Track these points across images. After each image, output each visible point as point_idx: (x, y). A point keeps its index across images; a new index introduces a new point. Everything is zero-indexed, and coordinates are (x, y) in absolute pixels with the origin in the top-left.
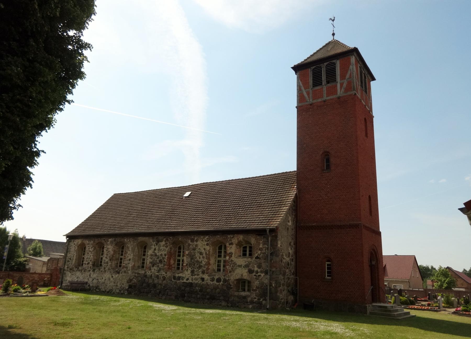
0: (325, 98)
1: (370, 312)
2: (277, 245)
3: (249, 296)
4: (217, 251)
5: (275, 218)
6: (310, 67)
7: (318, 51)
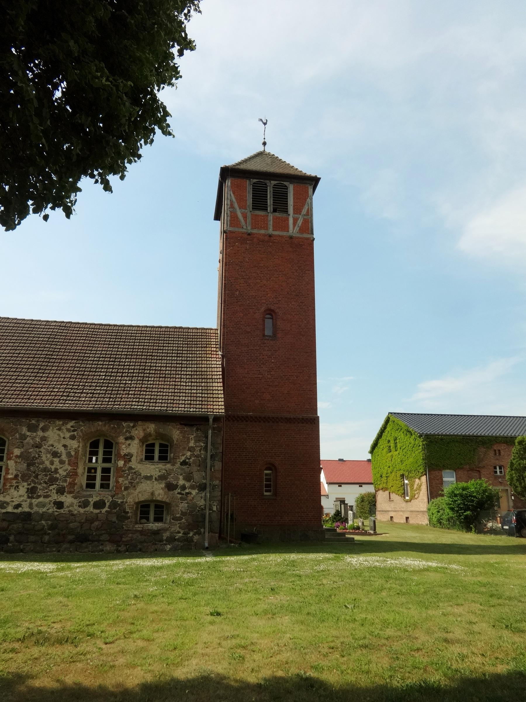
0: (271, 231)
3: (165, 530)
4: (88, 449)
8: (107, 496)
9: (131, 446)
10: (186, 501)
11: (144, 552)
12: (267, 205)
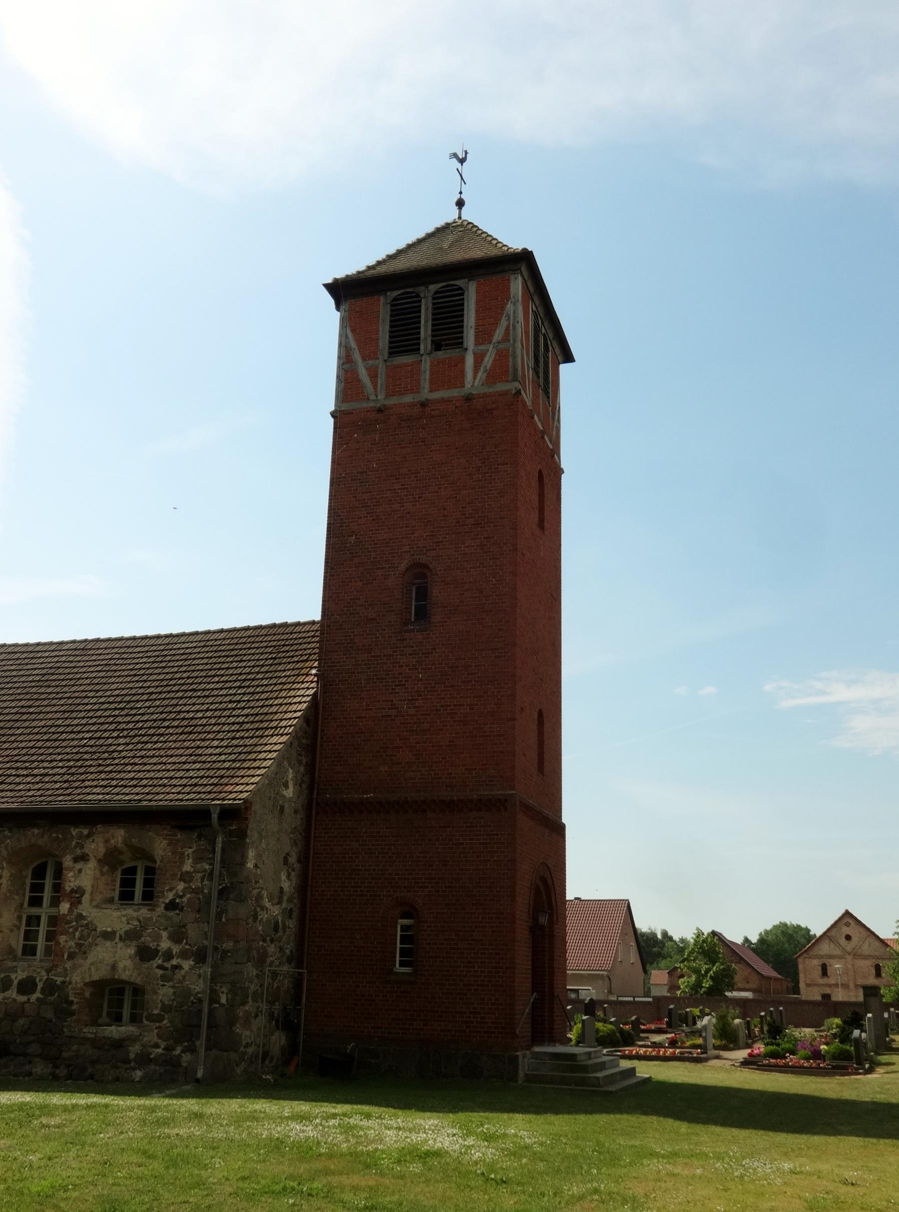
0: (426, 393)
1: (526, 1075)
2: (243, 864)
3: (133, 1039)
4: (28, 881)
5: (242, 772)
6: (383, 292)
7: (410, 246)
8: (39, 970)
9: (83, 874)
10: (171, 983)
11: (96, 1081)
12: (419, 338)
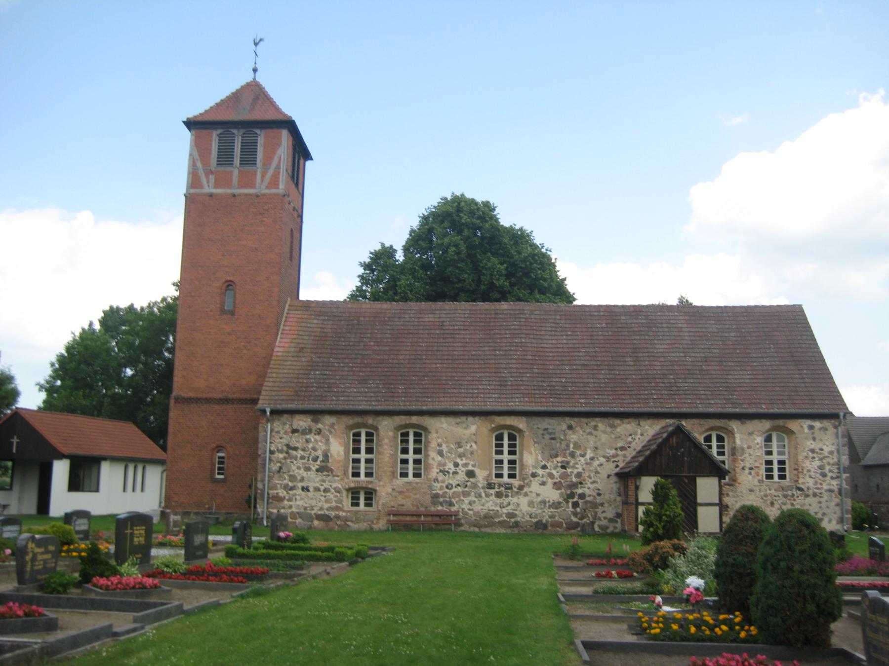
6: (216, 129)
